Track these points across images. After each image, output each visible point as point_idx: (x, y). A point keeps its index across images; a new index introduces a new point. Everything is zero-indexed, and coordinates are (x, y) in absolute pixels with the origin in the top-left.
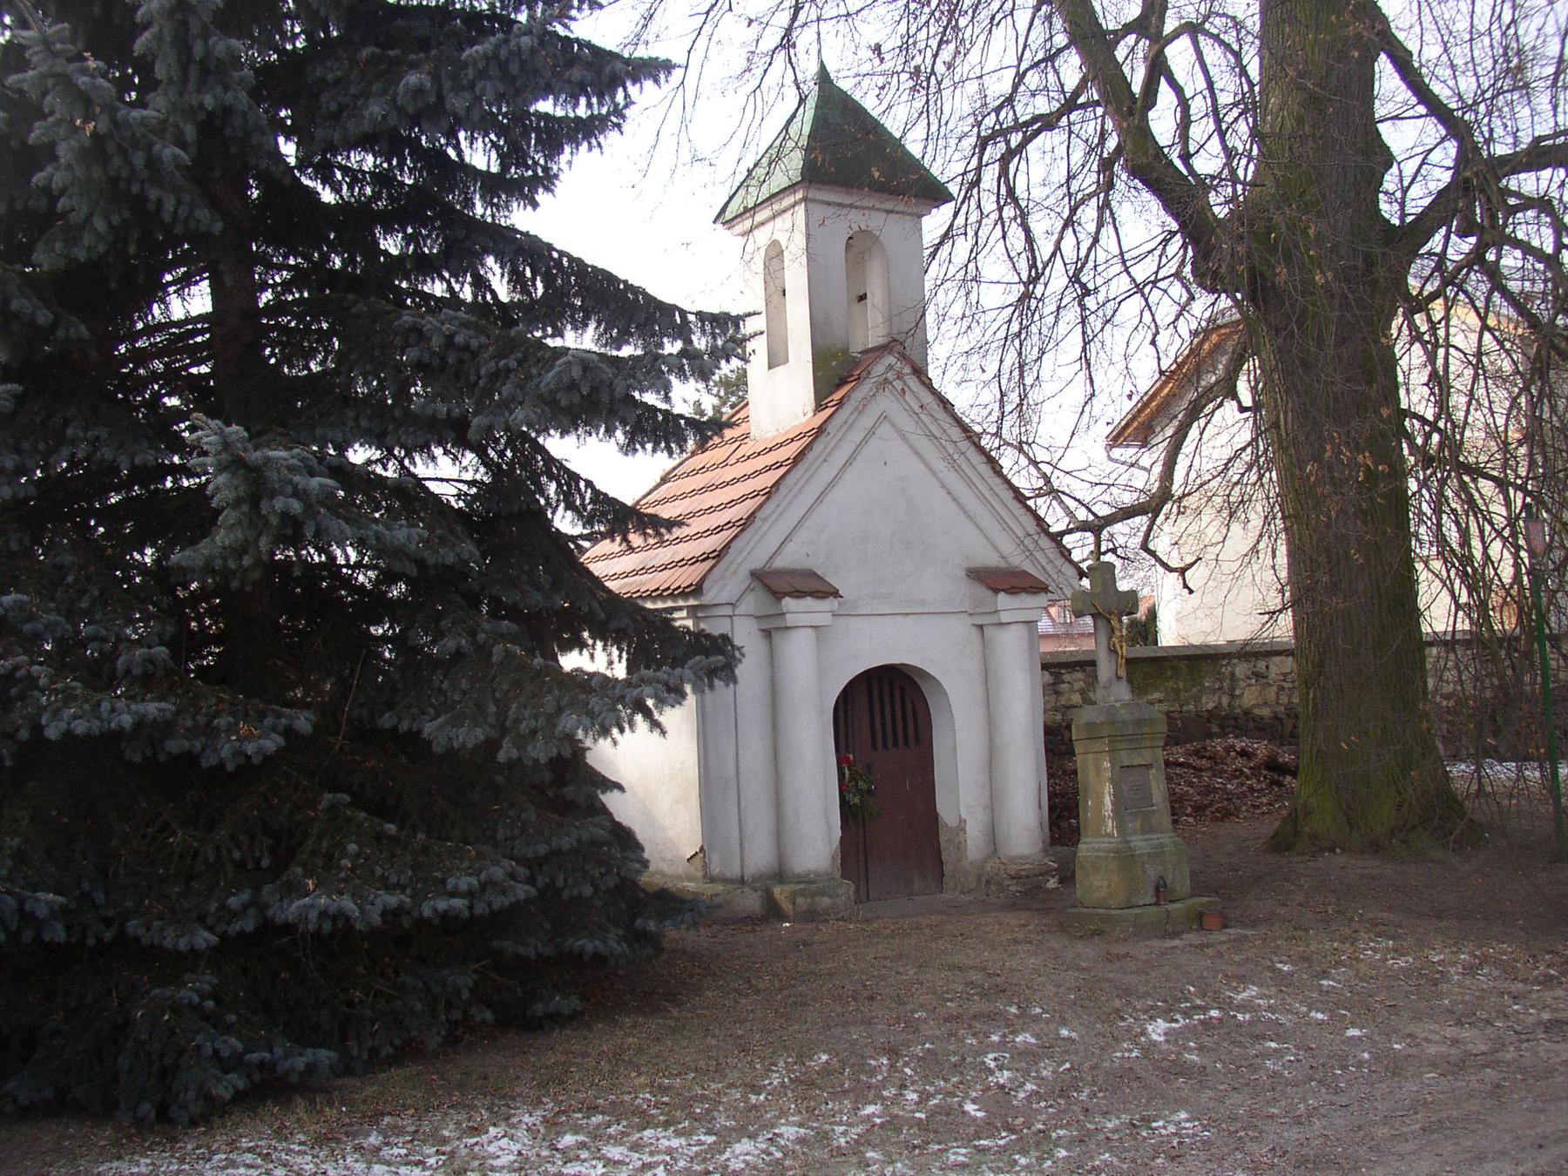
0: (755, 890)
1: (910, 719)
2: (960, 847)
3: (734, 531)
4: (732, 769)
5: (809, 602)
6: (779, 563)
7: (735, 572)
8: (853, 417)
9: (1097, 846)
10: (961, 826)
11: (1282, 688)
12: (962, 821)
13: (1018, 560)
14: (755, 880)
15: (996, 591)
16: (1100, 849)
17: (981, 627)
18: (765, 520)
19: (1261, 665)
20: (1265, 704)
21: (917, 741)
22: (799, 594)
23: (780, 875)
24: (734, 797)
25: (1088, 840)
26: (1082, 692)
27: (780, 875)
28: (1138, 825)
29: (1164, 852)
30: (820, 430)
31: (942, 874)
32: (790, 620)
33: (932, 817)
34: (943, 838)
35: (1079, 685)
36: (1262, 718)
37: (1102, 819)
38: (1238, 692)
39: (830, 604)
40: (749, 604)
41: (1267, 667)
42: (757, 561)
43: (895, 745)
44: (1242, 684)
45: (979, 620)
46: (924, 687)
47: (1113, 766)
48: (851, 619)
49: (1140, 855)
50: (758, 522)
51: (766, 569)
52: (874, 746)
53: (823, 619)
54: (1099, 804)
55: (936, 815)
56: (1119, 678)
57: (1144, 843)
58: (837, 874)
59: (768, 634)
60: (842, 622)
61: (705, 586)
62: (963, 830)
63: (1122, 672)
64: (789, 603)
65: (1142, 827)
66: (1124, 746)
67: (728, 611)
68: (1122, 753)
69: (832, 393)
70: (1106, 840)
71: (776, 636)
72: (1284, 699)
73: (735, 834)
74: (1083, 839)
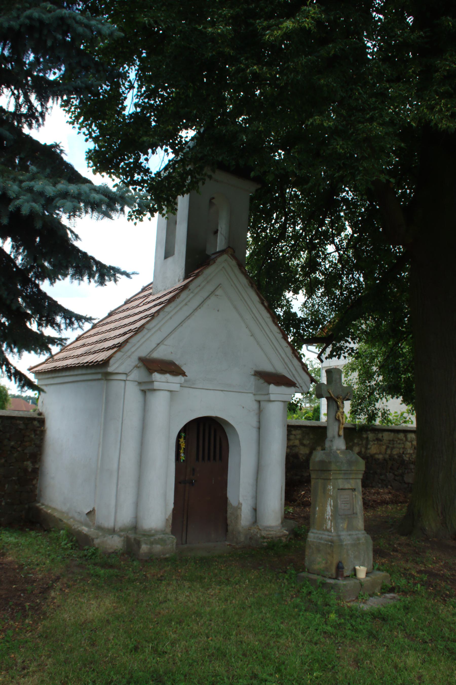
0: (120, 536)
1: (218, 446)
2: (237, 518)
3: (132, 334)
4: (115, 466)
5: (168, 377)
6: (156, 355)
7: (129, 357)
8: (203, 284)
9: (320, 536)
10: (239, 507)
11: (388, 447)
12: (240, 504)
13: (281, 369)
14: (122, 530)
15: (269, 383)
16: (321, 539)
17: (259, 402)
18: (149, 330)
19: (380, 435)
20: (380, 453)
21: (220, 458)
22: (163, 371)
23: (135, 528)
24: (115, 481)
25: (315, 531)
26: (300, 440)
27: (135, 528)
28: (345, 526)
29: (359, 543)
30: (185, 288)
31: (227, 530)
32: (156, 385)
33: (225, 500)
34: (229, 511)
35: (298, 437)
36: (379, 459)
37: (324, 520)
38: (369, 447)
39: (180, 379)
40: (135, 375)
41: (382, 436)
42: (143, 353)
43: (209, 459)
44: (371, 443)
45: (259, 398)
46: (227, 430)
47: (334, 488)
48: (191, 390)
49: (346, 545)
50: (145, 331)
51: (147, 357)
52: (198, 459)
53: (176, 387)
54: (323, 511)
55: (226, 499)
56: (339, 436)
57: (348, 537)
58: (169, 530)
59: (144, 392)
60: (186, 390)
61: (111, 361)
62: (240, 508)
63: (342, 433)
64: (157, 376)
65: (347, 527)
66: (341, 476)
67: (123, 377)
68: (340, 481)
69: (195, 270)
70: (326, 533)
71: (148, 394)
72: (389, 452)
73: (113, 503)
74: (312, 530)
